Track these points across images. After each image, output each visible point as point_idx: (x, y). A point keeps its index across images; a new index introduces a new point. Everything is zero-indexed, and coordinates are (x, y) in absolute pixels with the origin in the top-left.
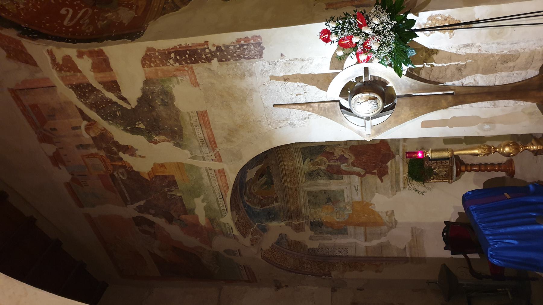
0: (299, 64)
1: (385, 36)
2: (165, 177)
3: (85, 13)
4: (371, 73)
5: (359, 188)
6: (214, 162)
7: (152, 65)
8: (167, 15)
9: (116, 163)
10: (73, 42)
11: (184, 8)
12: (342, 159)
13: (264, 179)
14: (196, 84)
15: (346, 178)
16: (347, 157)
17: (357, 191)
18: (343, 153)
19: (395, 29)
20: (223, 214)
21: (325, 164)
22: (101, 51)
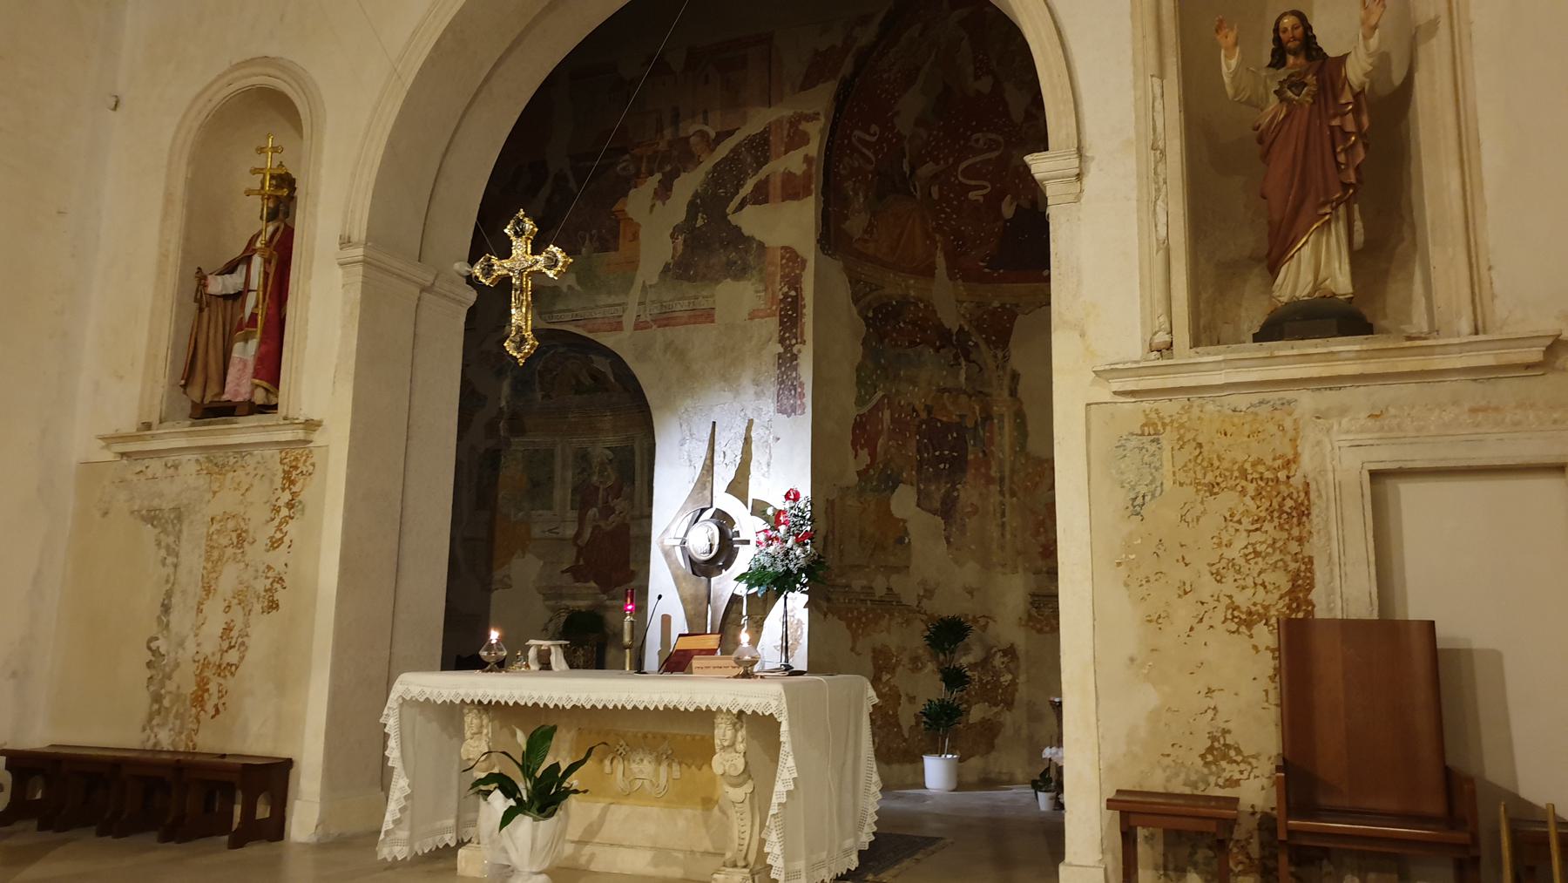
0: (764, 461)
1: (782, 561)
2: (616, 237)
3: (869, 161)
4: (742, 549)
5: (555, 535)
6: (634, 318)
7: (784, 261)
8: (849, 285)
9: (644, 165)
10: (828, 149)
11: (855, 310)
12: (608, 511)
13: (588, 381)
14: (752, 316)
15: (572, 515)
16: (611, 518)
17: (548, 531)
18: (617, 512)
19: (788, 572)
20: (543, 316)
21: (601, 482)
22: (810, 194)
